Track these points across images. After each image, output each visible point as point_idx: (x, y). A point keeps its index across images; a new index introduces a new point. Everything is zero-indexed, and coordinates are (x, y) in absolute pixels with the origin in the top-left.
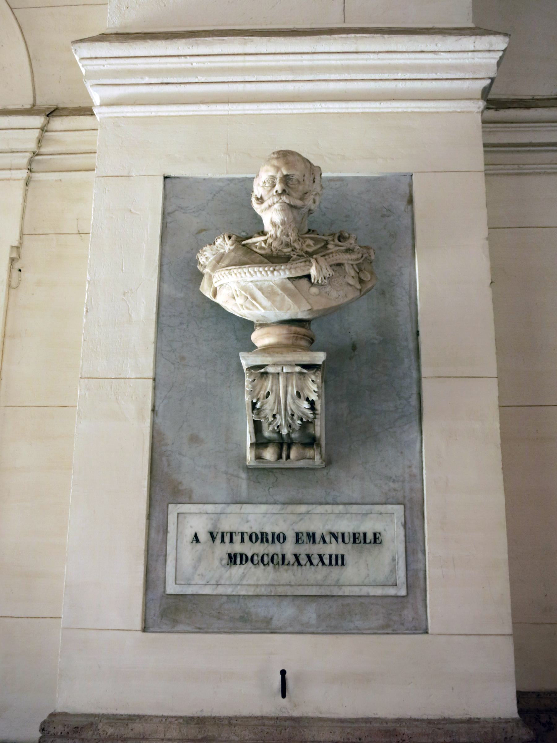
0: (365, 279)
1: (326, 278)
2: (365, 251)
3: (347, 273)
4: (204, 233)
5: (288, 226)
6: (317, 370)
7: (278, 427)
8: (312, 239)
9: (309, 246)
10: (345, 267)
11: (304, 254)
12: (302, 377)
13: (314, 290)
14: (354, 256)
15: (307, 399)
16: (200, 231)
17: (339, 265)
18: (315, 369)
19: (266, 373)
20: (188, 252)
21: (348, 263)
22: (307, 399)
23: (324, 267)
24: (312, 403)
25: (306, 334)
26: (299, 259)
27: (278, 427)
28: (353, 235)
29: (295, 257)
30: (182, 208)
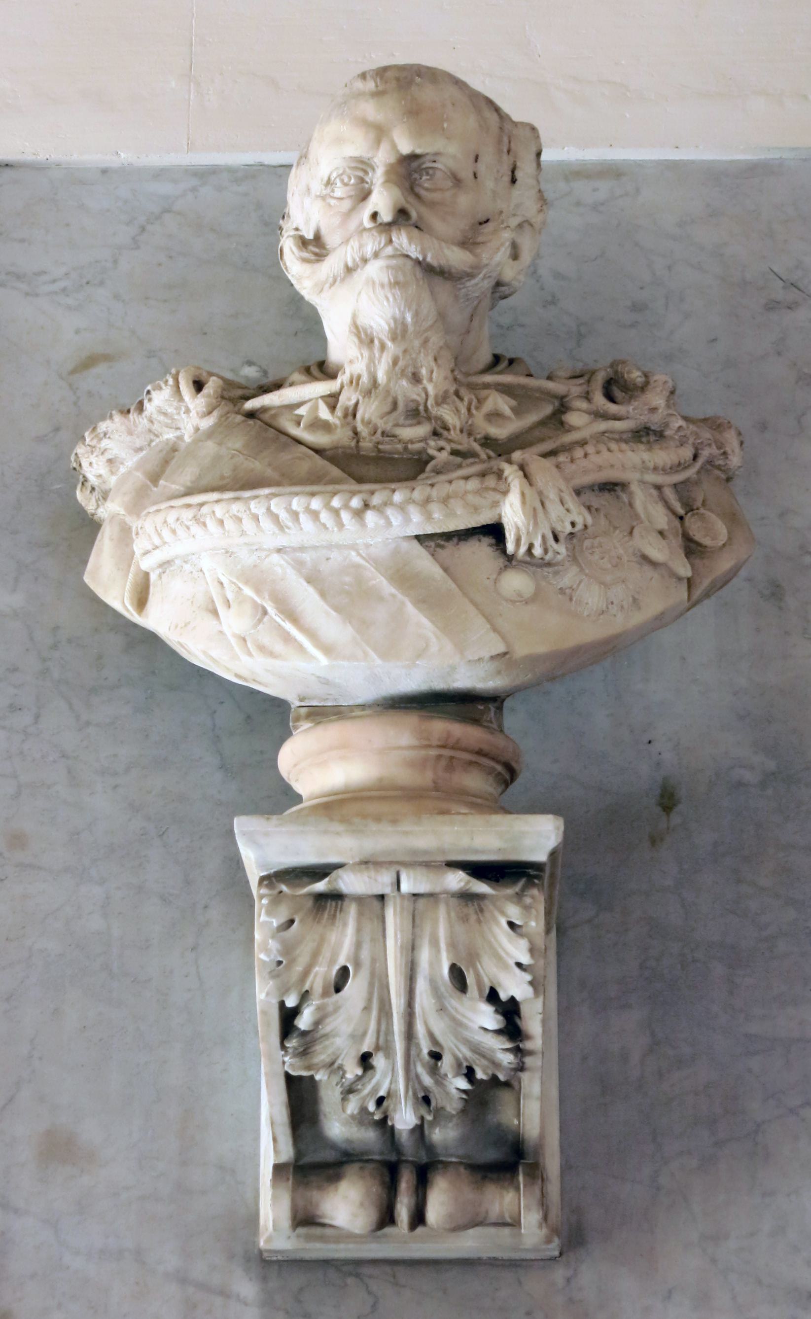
0: (707, 541)
1: (562, 537)
2: (706, 434)
3: (637, 516)
4: (101, 369)
5: (417, 343)
6: (530, 884)
7: (380, 1101)
8: (506, 390)
9: (495, 416)
10: (631, 495)
11: (477, 447)
12: (471, 910)
13: (516, 582)
14: (662, 456)
15: (493, 996)
16: (90, 362)
17: (610, 487)
18: (523, 882)
19: (337, 896)
20: (40, 439)
21: (642, 482)
22: (493, 996)
23: (552, 495)
24: (510, 1011)
25: (485, 747)
26: (460, 466)
27: (380, 1101)
28: (659, 377)
29: (443, 456)
30: (19, 277)
